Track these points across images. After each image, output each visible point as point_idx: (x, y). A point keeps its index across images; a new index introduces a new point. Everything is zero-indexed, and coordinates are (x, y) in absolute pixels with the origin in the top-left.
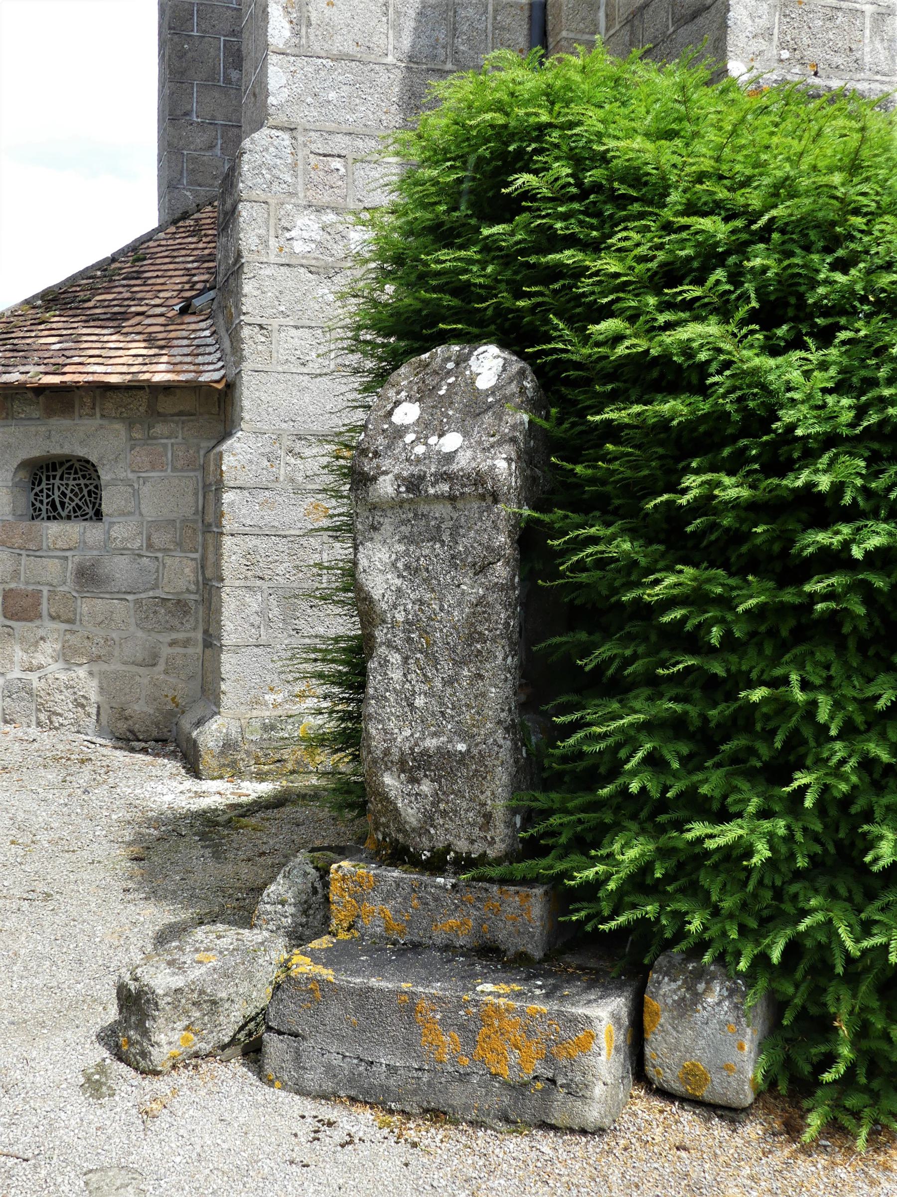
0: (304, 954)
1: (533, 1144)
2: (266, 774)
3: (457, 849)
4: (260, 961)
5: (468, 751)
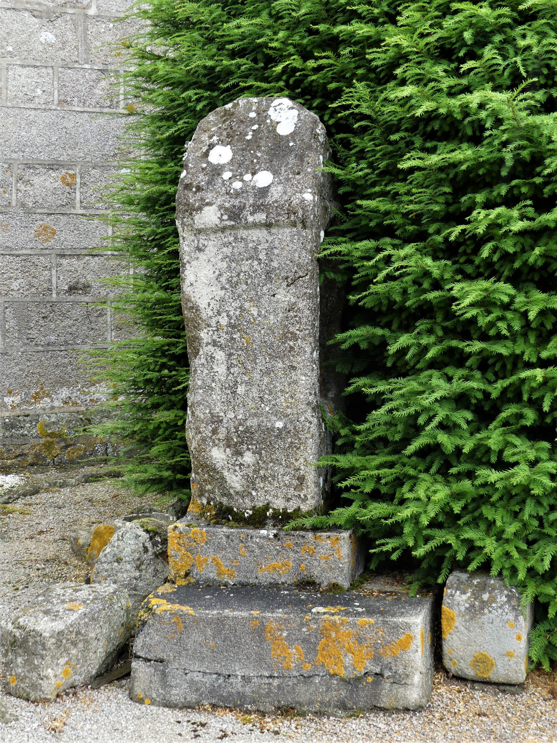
0: (158, 597)
1: (370, 722)
2: (9, 467)
3: (275, 507)
4: (116, 607)
5: (285, 427)
